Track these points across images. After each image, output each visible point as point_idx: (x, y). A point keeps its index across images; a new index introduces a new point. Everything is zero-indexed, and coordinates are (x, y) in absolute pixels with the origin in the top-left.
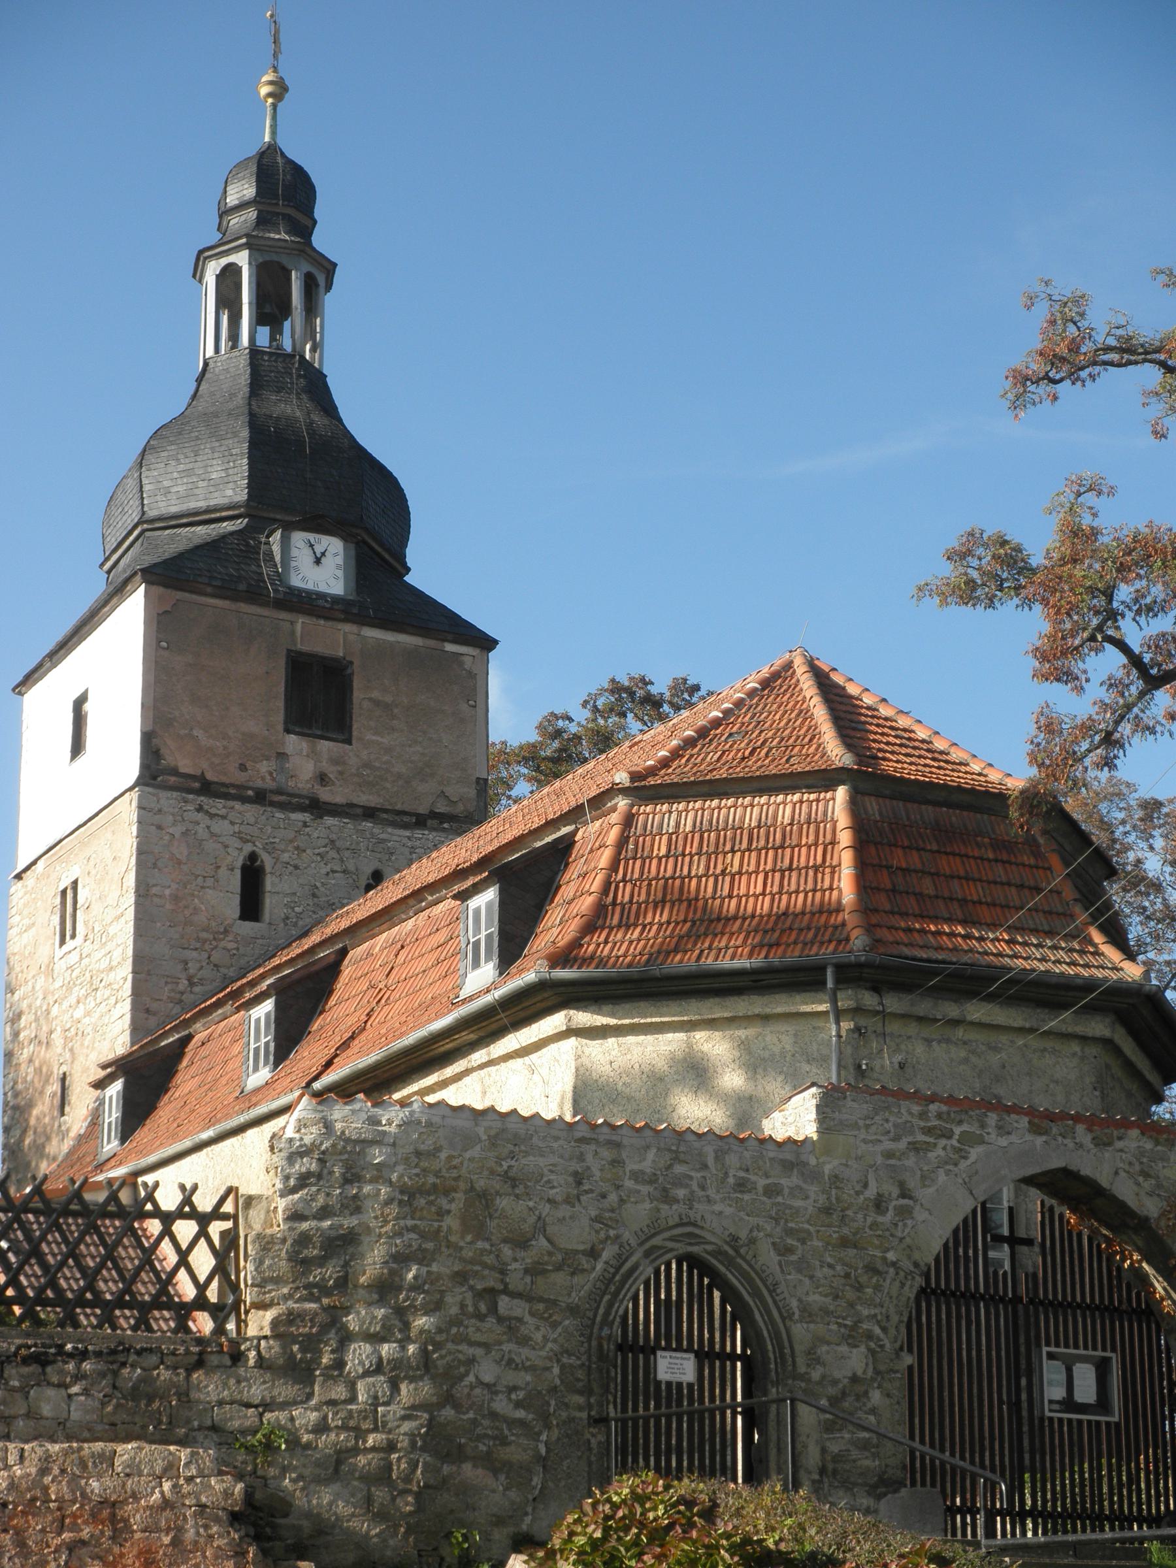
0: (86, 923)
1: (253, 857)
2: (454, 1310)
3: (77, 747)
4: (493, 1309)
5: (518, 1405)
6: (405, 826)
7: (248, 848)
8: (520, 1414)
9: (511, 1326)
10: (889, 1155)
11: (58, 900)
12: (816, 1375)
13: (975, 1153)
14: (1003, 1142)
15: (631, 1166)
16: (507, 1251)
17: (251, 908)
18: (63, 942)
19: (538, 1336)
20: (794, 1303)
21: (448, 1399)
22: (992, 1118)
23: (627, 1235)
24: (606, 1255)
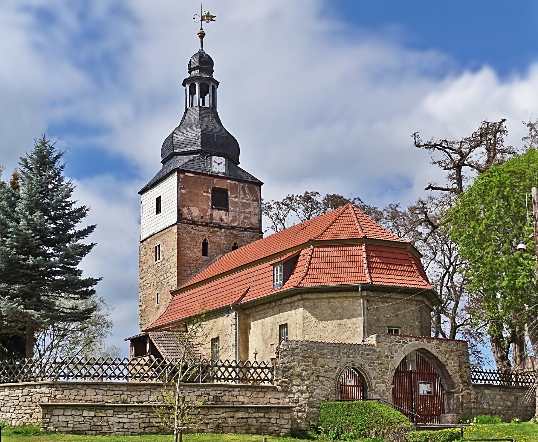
0: (163, 256)
1: (205, 240)
2: (312, 380)
3: (158, 211)
4: (319, 379)
5: (324, 397)
6: (242, 231)
7: (204, 238)
8: (324, 399)
9: (322, 382)
10: (389, 347)
11: (154, 249)
12: (376, 390)
13: (405, 345)
14: (410, 343)
15: (342, 351)
16: (321, 368)
17: (205, 253)
18: (156, 260)
19: (326, 384)
20: (372, 376)
21: (311, 396)
22: (408, 339)
23: (342, 364)
24: (338, 368)
